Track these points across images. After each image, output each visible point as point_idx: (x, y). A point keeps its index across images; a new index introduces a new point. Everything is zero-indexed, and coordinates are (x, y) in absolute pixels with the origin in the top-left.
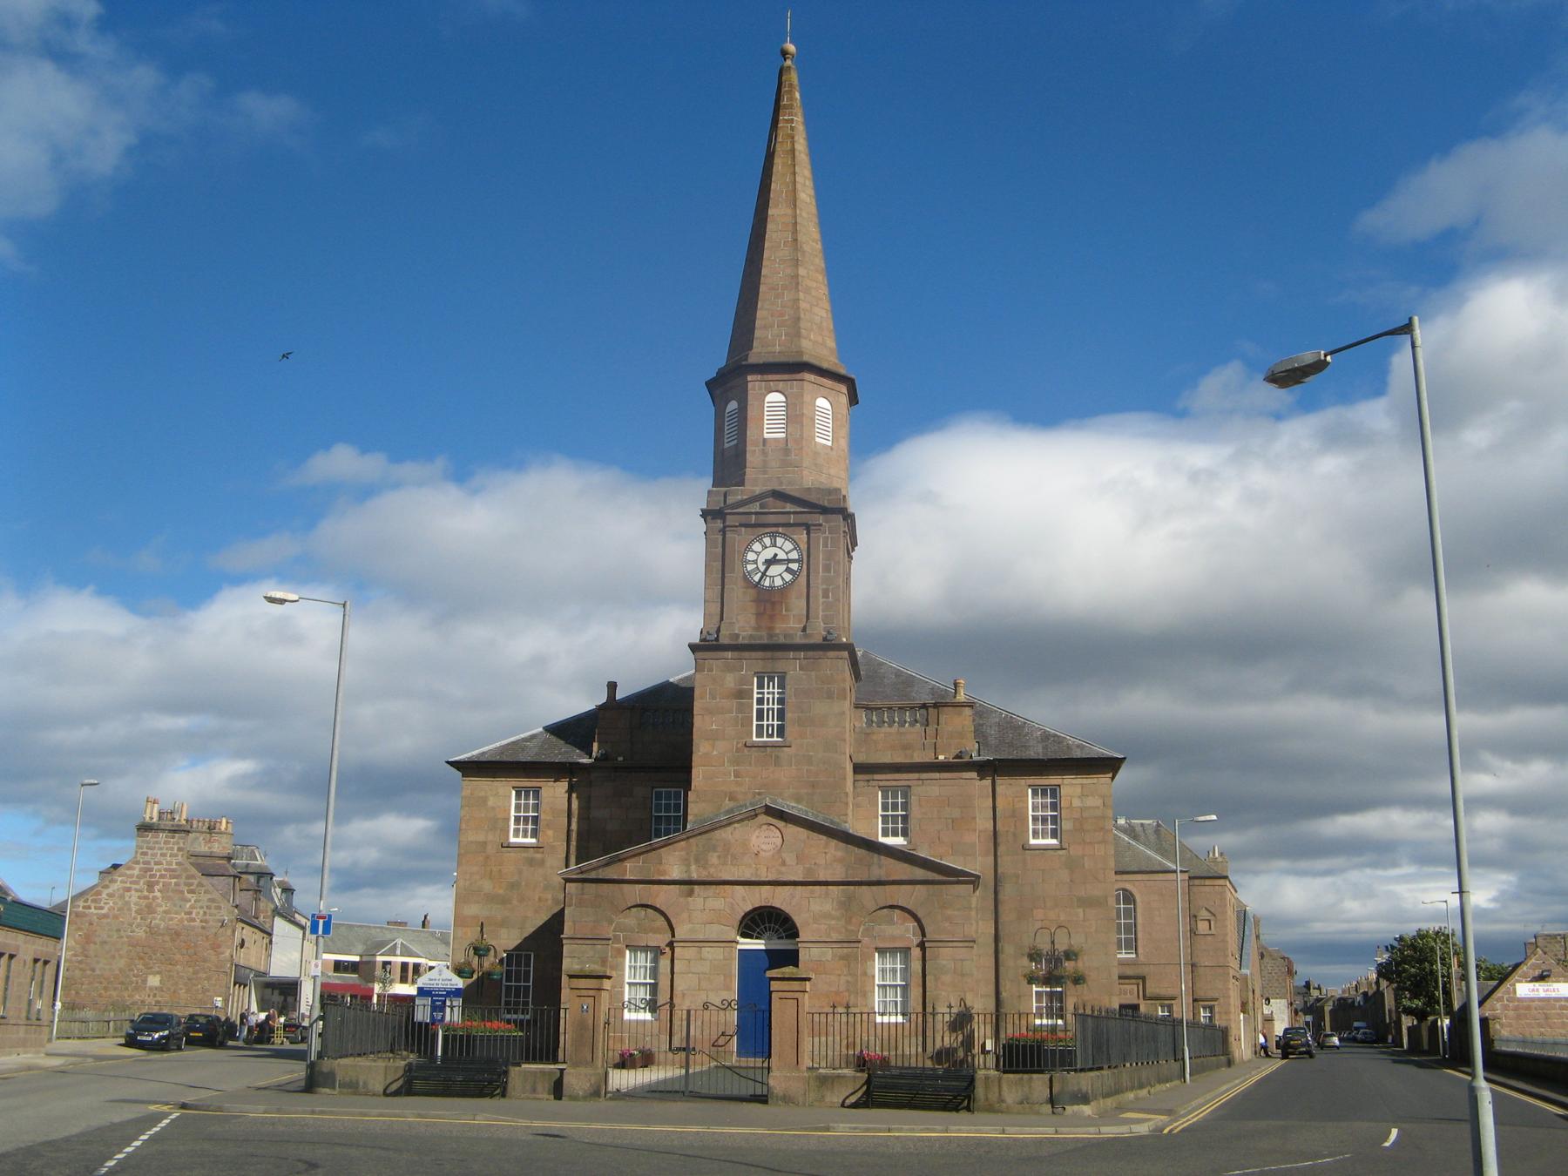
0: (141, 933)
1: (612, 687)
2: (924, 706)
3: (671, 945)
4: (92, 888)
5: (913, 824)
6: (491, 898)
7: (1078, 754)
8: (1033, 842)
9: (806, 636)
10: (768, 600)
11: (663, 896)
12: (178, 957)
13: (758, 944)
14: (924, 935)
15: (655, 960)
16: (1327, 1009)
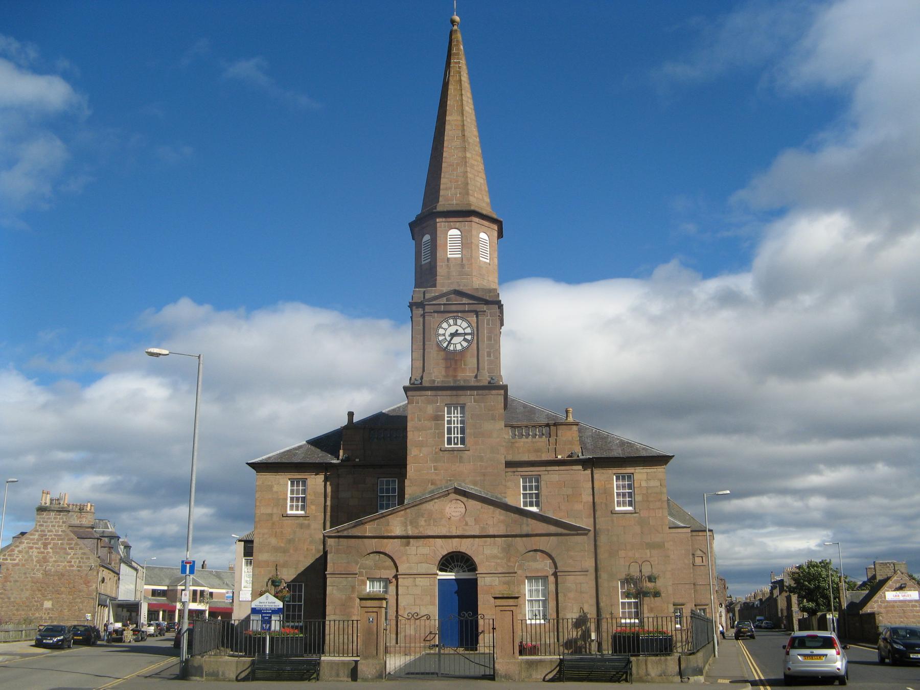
0: (39, 575)
1: (351, 415)
2: (548, 425)
3: (396, 577)
4: (8, 547)
5: (543, 499)
6: (276, 549)
7: (644, 454)
8: (617, 509)
9: (478, 381)
10: (453, 359)
11: (390, 546)
12: (62, 589)
13: (450, 576)
14: (556, 567)
15: (386, 587)
16: (737, 609)
